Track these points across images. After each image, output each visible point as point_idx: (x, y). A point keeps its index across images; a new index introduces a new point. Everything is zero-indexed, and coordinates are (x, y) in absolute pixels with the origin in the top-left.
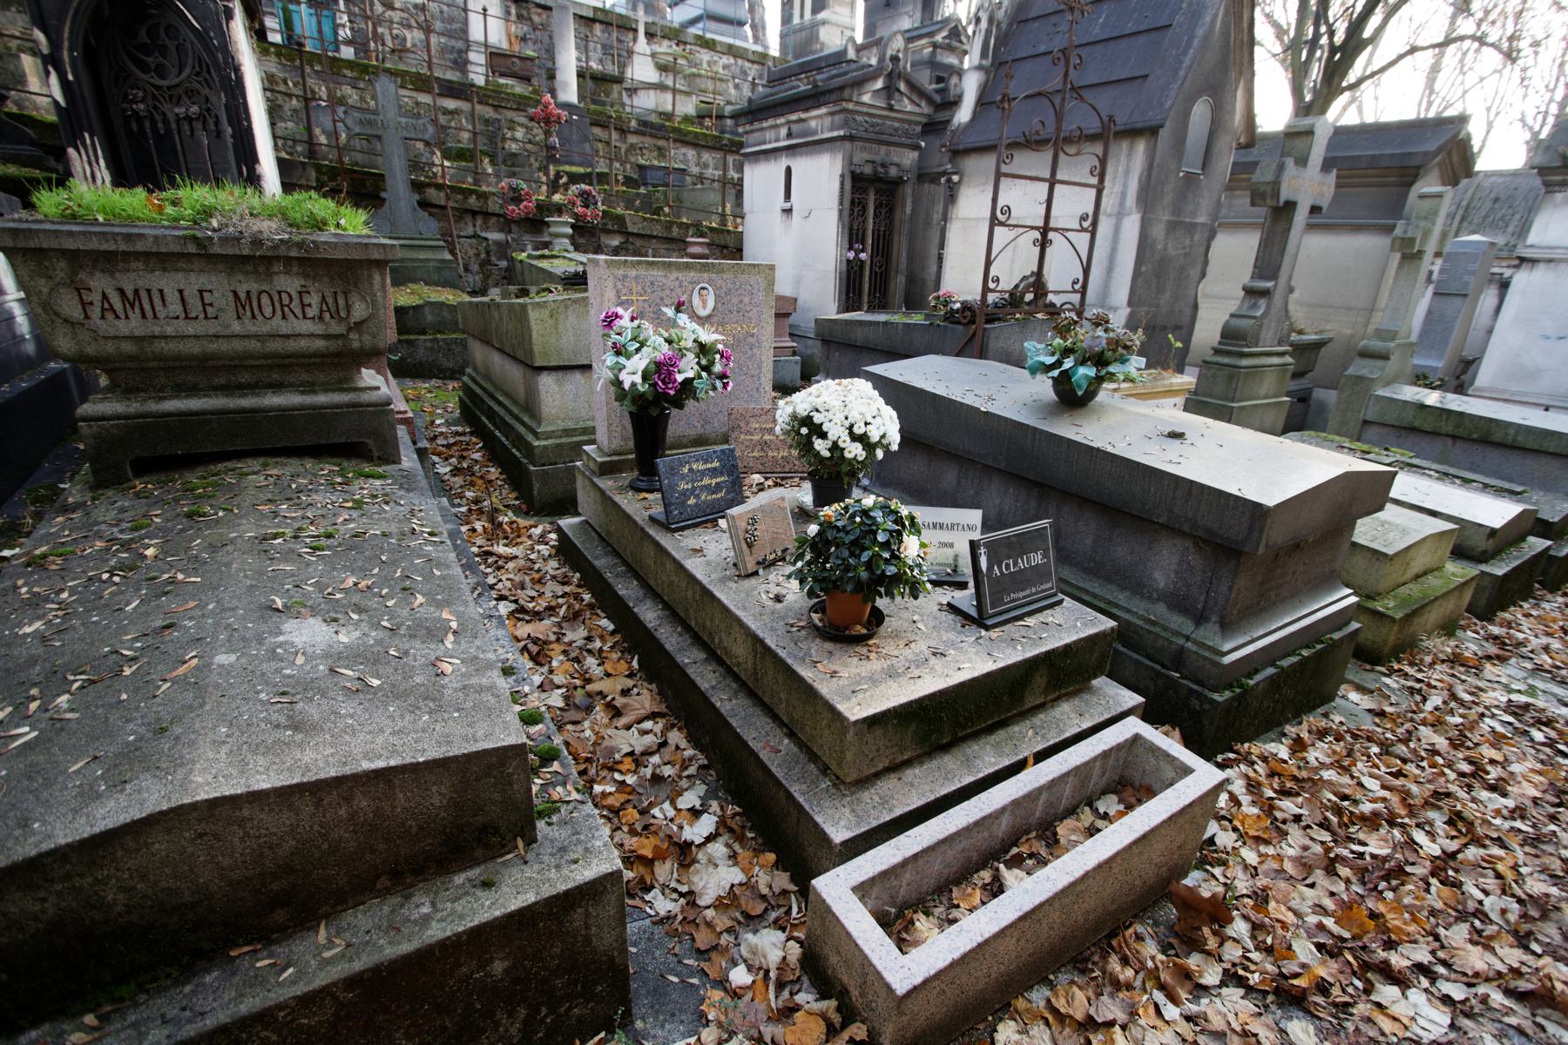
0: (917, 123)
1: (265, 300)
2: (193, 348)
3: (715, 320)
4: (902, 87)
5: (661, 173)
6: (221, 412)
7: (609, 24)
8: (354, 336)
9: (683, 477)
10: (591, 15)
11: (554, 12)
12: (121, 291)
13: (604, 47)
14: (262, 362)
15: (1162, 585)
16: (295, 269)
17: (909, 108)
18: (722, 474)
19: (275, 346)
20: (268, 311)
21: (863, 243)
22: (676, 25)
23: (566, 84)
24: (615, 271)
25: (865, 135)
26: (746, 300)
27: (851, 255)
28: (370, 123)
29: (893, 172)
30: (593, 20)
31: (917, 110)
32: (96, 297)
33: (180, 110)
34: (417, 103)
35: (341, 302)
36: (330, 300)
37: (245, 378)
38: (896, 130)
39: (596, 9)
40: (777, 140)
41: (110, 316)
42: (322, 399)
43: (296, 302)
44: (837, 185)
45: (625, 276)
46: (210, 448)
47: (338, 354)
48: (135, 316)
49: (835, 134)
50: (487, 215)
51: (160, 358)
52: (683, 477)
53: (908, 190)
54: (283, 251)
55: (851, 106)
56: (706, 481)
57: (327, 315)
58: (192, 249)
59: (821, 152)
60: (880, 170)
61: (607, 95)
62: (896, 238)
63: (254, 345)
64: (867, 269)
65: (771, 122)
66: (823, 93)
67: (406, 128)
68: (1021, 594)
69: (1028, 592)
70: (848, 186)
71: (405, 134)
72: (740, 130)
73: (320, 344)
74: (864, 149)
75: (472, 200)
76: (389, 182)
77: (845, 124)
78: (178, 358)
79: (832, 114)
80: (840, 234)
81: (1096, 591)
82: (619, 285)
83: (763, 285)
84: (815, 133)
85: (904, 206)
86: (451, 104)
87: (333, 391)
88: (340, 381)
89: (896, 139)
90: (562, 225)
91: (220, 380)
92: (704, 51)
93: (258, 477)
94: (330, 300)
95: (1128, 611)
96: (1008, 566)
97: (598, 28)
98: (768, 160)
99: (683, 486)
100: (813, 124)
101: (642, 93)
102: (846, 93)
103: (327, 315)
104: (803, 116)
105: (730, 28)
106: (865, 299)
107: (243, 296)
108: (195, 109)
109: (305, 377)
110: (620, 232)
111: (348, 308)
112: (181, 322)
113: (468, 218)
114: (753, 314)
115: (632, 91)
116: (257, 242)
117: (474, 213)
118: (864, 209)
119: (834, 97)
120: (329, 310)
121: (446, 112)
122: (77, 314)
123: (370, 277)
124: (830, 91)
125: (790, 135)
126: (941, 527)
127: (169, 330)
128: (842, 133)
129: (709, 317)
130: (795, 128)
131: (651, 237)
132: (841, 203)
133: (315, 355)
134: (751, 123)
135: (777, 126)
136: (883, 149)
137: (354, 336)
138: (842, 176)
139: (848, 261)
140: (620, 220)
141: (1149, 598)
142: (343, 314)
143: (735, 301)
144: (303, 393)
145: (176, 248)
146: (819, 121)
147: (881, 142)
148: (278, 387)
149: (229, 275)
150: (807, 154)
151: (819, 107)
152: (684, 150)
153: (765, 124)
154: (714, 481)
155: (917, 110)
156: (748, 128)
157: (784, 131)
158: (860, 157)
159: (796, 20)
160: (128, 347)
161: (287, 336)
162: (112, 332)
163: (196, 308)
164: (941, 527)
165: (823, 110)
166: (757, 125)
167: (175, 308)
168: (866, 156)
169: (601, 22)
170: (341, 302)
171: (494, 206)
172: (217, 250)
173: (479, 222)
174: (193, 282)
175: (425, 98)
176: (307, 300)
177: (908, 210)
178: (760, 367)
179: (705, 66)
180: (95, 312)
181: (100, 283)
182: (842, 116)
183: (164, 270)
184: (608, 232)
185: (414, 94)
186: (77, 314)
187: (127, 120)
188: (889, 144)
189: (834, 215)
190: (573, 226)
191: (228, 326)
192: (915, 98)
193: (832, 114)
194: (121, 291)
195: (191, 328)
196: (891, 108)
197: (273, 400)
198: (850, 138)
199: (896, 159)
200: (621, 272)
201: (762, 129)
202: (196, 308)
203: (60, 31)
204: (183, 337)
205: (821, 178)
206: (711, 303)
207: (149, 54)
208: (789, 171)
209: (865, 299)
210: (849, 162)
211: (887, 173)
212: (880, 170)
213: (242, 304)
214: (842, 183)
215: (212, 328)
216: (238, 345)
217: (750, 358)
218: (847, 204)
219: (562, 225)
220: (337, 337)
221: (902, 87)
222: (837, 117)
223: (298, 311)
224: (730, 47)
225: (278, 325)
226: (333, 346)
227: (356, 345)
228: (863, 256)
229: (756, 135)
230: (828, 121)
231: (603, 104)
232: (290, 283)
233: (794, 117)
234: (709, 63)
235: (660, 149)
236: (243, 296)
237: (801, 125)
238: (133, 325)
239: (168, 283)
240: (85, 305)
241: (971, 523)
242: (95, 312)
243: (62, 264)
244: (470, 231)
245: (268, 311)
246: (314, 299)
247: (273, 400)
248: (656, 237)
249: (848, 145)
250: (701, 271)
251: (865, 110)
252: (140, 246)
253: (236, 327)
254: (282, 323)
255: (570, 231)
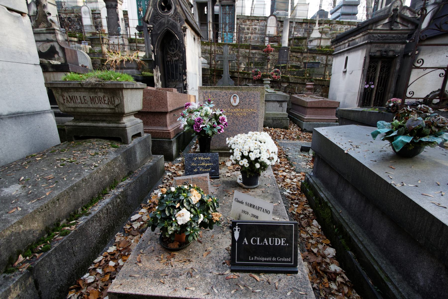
0: (405, 33)
1: (96, 99)
2: (84, 110)
3: (239, 107)
4: (398, 20)
5: (311, 64)
6: (106, 127)
7: (307, 23)
8: (116, 109)
9: (193, 161)
10: (302, 21)
11: (284, 22)
12: (70, 97)
13: (305, 30)
14: (99, 115)
15: (421, 284)
16: (102, 91)
17: (401, 28)
18: (210, 162)
19: (100, 111)
20: (97, 101)
21: (374, 81)
22: (331, 19)
23: (285, 41)
24: (203, 90)
25: (377, 41)
26: (252, 100)
27: (367, 86)
28: (221, 58)
29: (391, 54)
30: (303, 23)
31: (406, 28)
32: (65, 98)
33: (175, 59)
34: (246, 52)
35: (113, 99)
36: (110, 99)
37: (98, 118)
38: (394, 37)
39: (304, 19)
40: (344, 48)
41: (68, 102)
42: (111, 125)
43: (103, 100)
44: (362, 61)
45: (206, 92)
46: (87, 135)
47: (114, 113)
48: (72, 102)
49: (364, 42)
50: (249, 79)
51: (78, 112)
52: (193, 161)
53: (398, 60)
54: (97, 86)
55: (371, 31)
56: (203, 164)
57: (110, 103)
58: (80, 86)
59: (359, 50)
60: (384, 53)
61: (301, 43)
62: (390, 79)
63: (95, 110)
64: (375, 91)
65: (343, 42)
66: (361, 28)
67: (229, 58)
68: (263, 259)
69: (269, 259)
70: (368, 61)
71: (229, 59)
72: (333, 47)
73: (109, 110)
74: (376, 47)
75: (246, 75)
76: (224, 72)
77: (369, 38)
78: (81, 113)
79: (364, 35)
80: (363, 78)
81: (383, 266)
82: (204, 95)
83: (259, 95)
84: (358, 43)
85: (395, 66)
86: (254, 51)
87: (114, 123)
88: (118, 121)
89: (394, 41)
90: (267, 81)
91: (93, 119)
92: (338, 25)
93: (95, 142)
94: (110, 99)
95: (397, 288)
96: (255, 241)
97: (304, 25)
98: (341, 55)
99: (193, 164)
100: (357, 40)
101: (313, 41)
102: (370, 27)
103: (110, 103)
104: (353, 38)
105: (352, 16)
106: (372, 102)
107: (92, 98)
108: (177, 58)
109: (110, 119)
110: (287, 82)
111: (114, 101)
112: (80, 104)
113: (245, 80)
114: (255, 105)
115: (311, 41)
116: (91, 83)
117: (246, 79)
118: (375, 69)
119: (364, 29)
120: (111, 102)
121: (252, 53)
122: (63, 102)
123: (119, 93)
124: (364, 27)
125: (349, 46)
126: (254, 207)
127: (79, 106)
128: (366, 42)
129: (237, 106)
130: (351, 43)
131: (298, 83)
132: (364, 67)
133: (109, 113)
134: (337, 44)
135: (345, 43)
136: (386, 46)
137: (116, 109)
138: (365, 57)
139: (365, 89)
140: (288, 78)
141: (413, 287)
142: (113, 103)
143: (248, 100)
144: (108, 123)
145: (77, 86)
146: (359, 39)
147: (385, 43)
148: (103, 121)
149: (89, 92)
150: (354, 51)
151: (359, 34)
152: (322, 56)
153: (341, 43)
154: (206, 165)
155: (406, 28)
156: (336, 45)
157: (347, 45)
158: (373, 50)
159: (379, 9)
160: (72, 110)
161: (102, 108)
162: (69, 106)
163: (83, 101)
164: (254, 207)
165: (361, 35)
166: (338, 44)
167: (79, 101)
168: (377, 49)
169: (305, 23)
170: (113, 99)
171: (251, 76)
172: (84, 86)
173: (247, 81)
174: (82, 94)
175: (248, 51)
176: (105, 99)
177: (398, 68)
178: (257, 125)
179: (338, 30)
180: (66, 101)
181: (66, 95)
182: (368, 36)
183: (77, 91)
184: (284, 82)
185: (245, 50)
186: (63, 102)
187: (167, 62)
188: (389, 43)
189: (360, 72)
190: (271, 81)
191: (89, 105)
192: (405, 24)
193: (364, 35)
194: (70, 97)
195: (83, 106)
196: (392, 29)
197: (101, 124)
198: (371, 43)
199: (393, 49)
200: (205, 91)
201: (340, 45)
202: (83, 101)
203: (155, 44)
204: (82, 108)
205: (357, 59)
206: (238, 101)
207: (171, 47)
208: (347, 58)
209: (372, 102)
210: (369, 52)
211: (387, 54)
212: (384, 53)
213: (92, 100)
214: (365, 60)
215: (86, 106)
216: (92, 110)
217: (254, 121)
218: (366, 67)
219: (267, 81)
220: (113, 109)
221: (398, 20)
222: (366, 36)
223: (103, 102)
224: (349, 22)
225: (99, 105)
226: (112, 111)
227: (117, 111)
228: (372, 86)
229: (338, 47)
230: (362, 38)
231: (300, 46)
232: (101, 95)
233: (350, 39)
234: (340, 29)
235: (314, 57)
236: (92, 98)
237: (353, 42)
238: (72, 105)
239: (77, 94)
240: (64, 100)
241: (268, 209)
242: (66, 101)
243: (60, 91)
244: (245, 83)
245: (97, 101)
246: (106, 99)
247: (101, 124)
248: (299, 83)
249: (369, 46)
250: (234, 90)
251: (378, 32)
252: (71, 86)
253: (91, 106)
254: (100, 105)
255: (270, 82)
